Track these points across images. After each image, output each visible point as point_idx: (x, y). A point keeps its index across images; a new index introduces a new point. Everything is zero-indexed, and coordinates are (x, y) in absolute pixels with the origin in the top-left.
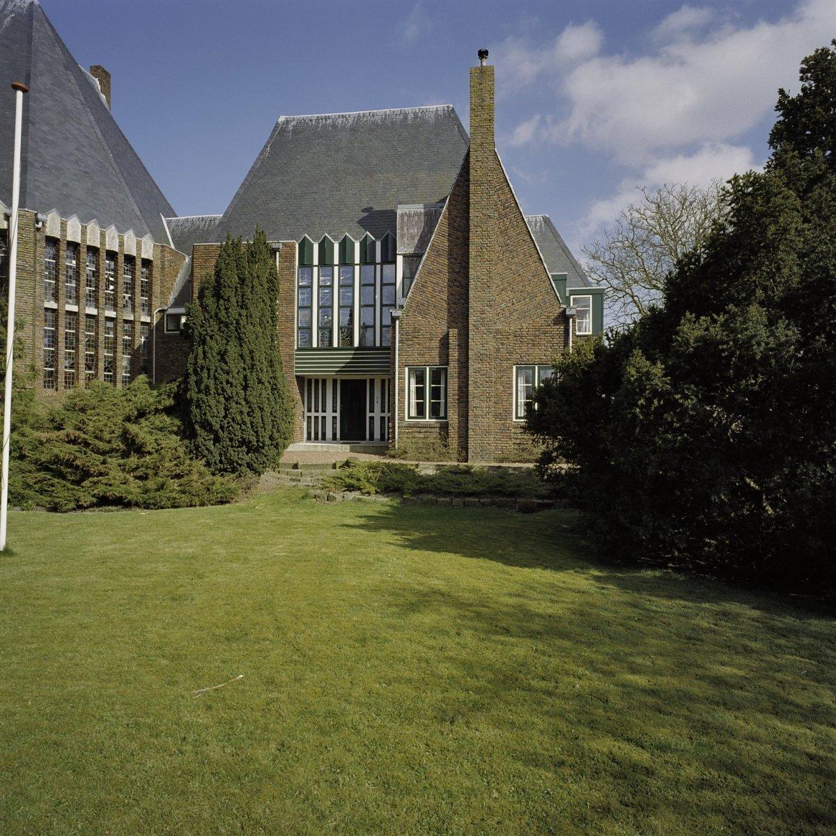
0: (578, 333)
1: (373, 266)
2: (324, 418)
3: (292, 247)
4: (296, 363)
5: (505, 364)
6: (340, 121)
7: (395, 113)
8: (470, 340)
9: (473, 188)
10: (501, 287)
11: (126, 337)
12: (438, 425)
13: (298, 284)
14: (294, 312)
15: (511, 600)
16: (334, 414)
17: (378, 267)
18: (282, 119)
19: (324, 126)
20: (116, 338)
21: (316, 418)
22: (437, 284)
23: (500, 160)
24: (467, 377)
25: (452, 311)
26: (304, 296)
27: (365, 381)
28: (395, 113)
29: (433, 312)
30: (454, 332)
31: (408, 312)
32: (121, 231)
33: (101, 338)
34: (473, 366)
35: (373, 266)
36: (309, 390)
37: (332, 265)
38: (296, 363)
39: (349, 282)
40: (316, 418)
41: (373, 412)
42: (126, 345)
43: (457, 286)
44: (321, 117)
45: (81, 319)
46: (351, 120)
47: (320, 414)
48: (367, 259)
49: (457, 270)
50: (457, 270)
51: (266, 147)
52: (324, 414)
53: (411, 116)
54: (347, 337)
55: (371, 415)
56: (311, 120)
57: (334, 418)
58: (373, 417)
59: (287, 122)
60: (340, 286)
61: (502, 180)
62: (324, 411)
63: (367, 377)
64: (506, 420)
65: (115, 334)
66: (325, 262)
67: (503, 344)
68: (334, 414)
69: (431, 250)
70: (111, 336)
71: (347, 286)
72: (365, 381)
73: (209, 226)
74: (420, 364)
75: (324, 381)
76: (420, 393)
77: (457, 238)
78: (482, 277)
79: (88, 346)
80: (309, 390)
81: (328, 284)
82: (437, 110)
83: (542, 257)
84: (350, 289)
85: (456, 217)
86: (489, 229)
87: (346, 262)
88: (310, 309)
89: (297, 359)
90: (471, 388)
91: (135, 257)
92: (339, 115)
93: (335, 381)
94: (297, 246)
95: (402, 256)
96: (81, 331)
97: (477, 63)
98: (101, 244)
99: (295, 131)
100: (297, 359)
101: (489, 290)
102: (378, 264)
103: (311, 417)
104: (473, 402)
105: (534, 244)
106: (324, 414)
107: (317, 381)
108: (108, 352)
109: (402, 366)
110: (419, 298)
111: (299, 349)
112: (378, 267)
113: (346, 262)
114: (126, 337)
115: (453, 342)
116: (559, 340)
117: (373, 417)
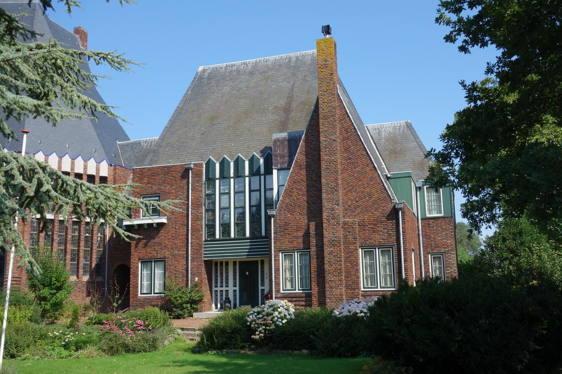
0: (428, 215)
1: (258, 177)
2: (227, 291)
3: (201, 165)
4: (205, 251)
5: (352, 247)
6: (242, 67)
7: (283, 58)
8: (324, 230)
9: (321, 121)
10: (348, 190)
11: (87, 235)
12: (304, 295)
13: (205, 192)
14: (202, 213)
15: (27, 290)
16: (235, 288)
17: (262, 177)
18: (201, 69)
19: (231, 72)
20: (79, 235)
21: (221, 291)
22: (301, 190)
23: (342, 99)
24: (323, 258)
25: (312, 208)
26: (209, 201)
27: (258, 261)
28: (283, 58)
29: (298, 210)
30: (312, 225)
31: (280, 211)
32: (86, 161)
33: (69, 237)
34: (327, 250)
35: (258, 177)
36: (222, 269)
37: (229, 178)
38: (205, 251)
39: (242, 189)
40: (221, 291)
41: (228, 287)
42: (87, 240)
43: (315, 191)
44: (232, 64)
45: (56, 224)
46: (250, 66)
47: (224, 289)
48: (255, 172)
49: (314, 179)
50: (314, 179)
51: (188, 90)
52: (227, 289)
53: (294, 60)
54: (240, 230)
55: (263, 288)
56: (222, 68)
57: (235, 291)
58: (228, 291)
59: (204, 71)
60: (235, 193)
61: (344, 113)
62: (227, 286)
63: (259, 259)
64: (354, 289)
65: (79, 232)
66: (224, 176)
67: (349, 232)
68: (235, 288)
69: (295, 165)
70: (77, 234)
71: (240, 192)
72: (258, 261)
73: (150, 146)
74: (286, 249)
75: (227, 263)
76: (291, 269)
77: (314, 156)
78: (331, 184)
79: (59, 243)
80: (222, 269)
81: (227, 191)
82: (313, 54)
83: (376, 166)
84: (243, 194)
85: (312, 141)
86: (334, 149)
87: (239, 175)
88: (244, 193)
89: (205, 248)
90: (326, 266)
91: (95, 175)
92: (242, 63)
93: (235, 263)
94: (204, 165)
95: (276, 170)
96: (55, 233)
97: (322, 36)
98: (71, 169)
99: (209, 78)
100: (205, 248)
101: (336, 193)
102: (262, 175)
103: (217, 291)
104: (329, 277)
105: (370, 157)
106: (227, 289)
107: (221, 263)
108: (74, 247)
109: (278, 251)
110: (287, 201)
111: (206, 241)
112: (262, 177)
113: (239, 175)
114: (87, 235)
115: (312, 231)
116: (392, 227)
117: (228, 291)
